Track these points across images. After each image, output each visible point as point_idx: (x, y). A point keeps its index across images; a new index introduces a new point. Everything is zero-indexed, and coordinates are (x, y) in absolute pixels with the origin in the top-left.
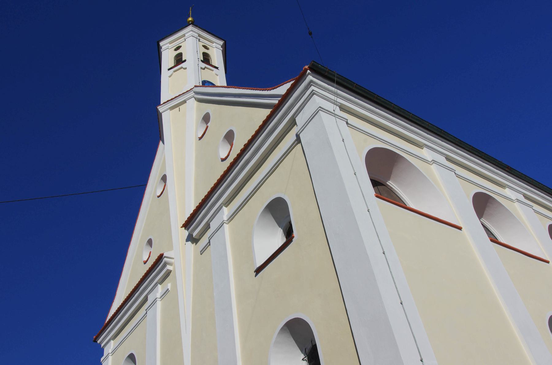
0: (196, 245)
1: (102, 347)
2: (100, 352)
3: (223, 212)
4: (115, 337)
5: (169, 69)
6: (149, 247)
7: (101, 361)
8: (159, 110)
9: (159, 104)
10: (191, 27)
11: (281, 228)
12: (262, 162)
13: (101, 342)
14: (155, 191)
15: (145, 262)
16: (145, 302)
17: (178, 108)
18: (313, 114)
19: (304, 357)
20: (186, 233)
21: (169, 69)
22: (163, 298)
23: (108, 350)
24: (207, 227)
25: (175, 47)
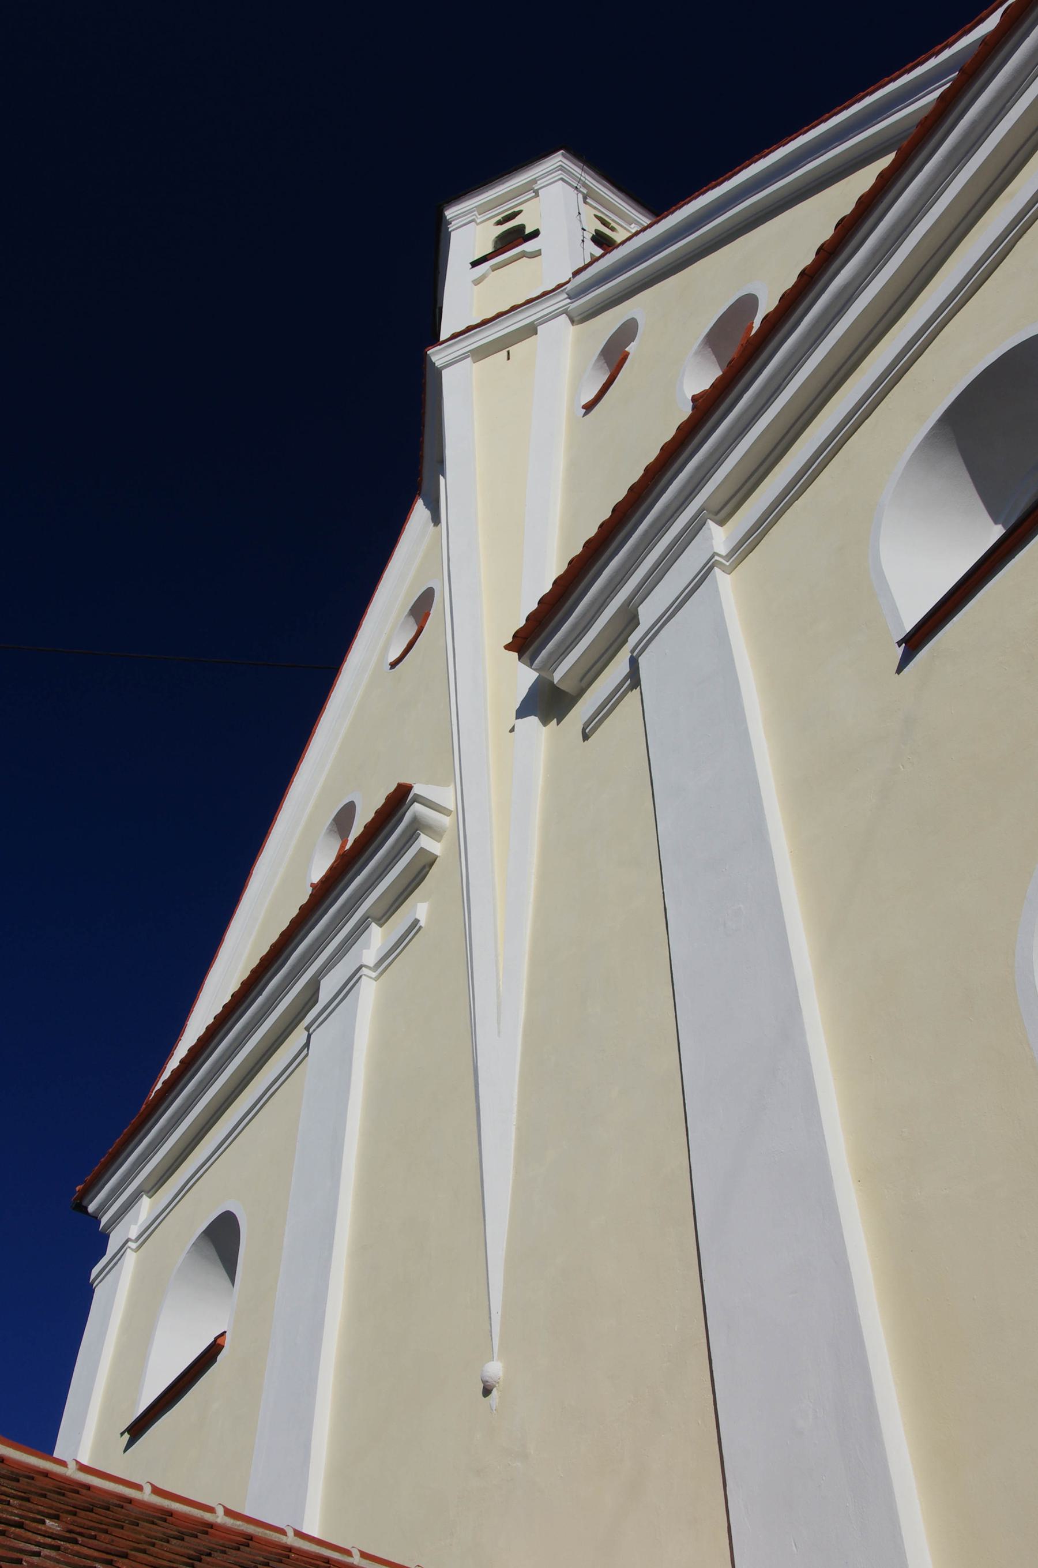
0: (558, 725)
5: (475, 264)
7: (93, 1276)
8: (434, 359)
9: (434, 339)
10: (561, 158)
12: (953, 238)
13: (103, 1207)
14: (385, 650)
17: (504, 353)
18: (165, 1218)
20: (525, 677)
21: (475, 264)
25: (499, 218)
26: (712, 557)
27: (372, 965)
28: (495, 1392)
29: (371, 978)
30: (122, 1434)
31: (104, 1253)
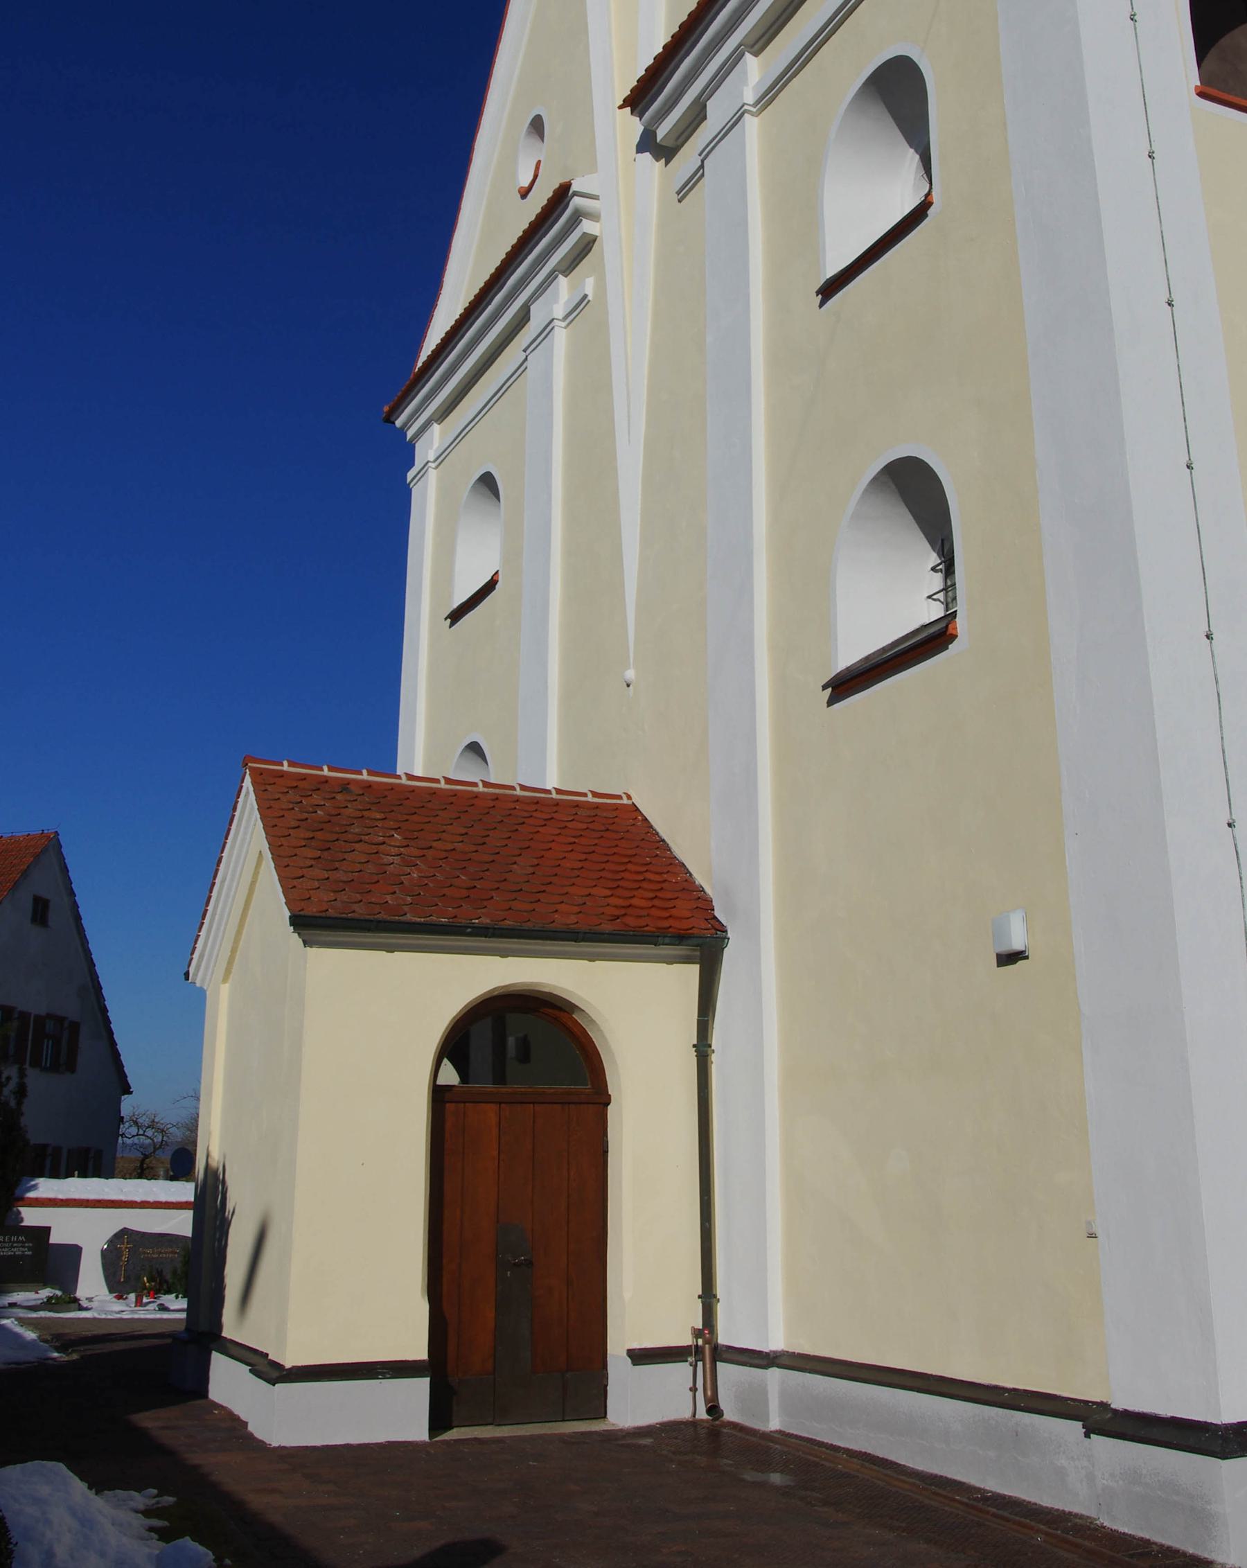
1: (408, 439)
2: (405, 453)
3: (745, 73)
4: (444, 413)
6: (535, 140)
7: (409, 480)
11: (917, 152)
13: (407, 424)
15: (525, 193)
16: (522, 324)
19: (939, 561)
20: (634, 127)
22: (573, 320)
23: (429, 446)
24: (698, 114)
26: (743, 106)
27: (561, 318)
28: (631, 685)
29: (562, 327)
30: (446, 619)
31: (413, 465)
